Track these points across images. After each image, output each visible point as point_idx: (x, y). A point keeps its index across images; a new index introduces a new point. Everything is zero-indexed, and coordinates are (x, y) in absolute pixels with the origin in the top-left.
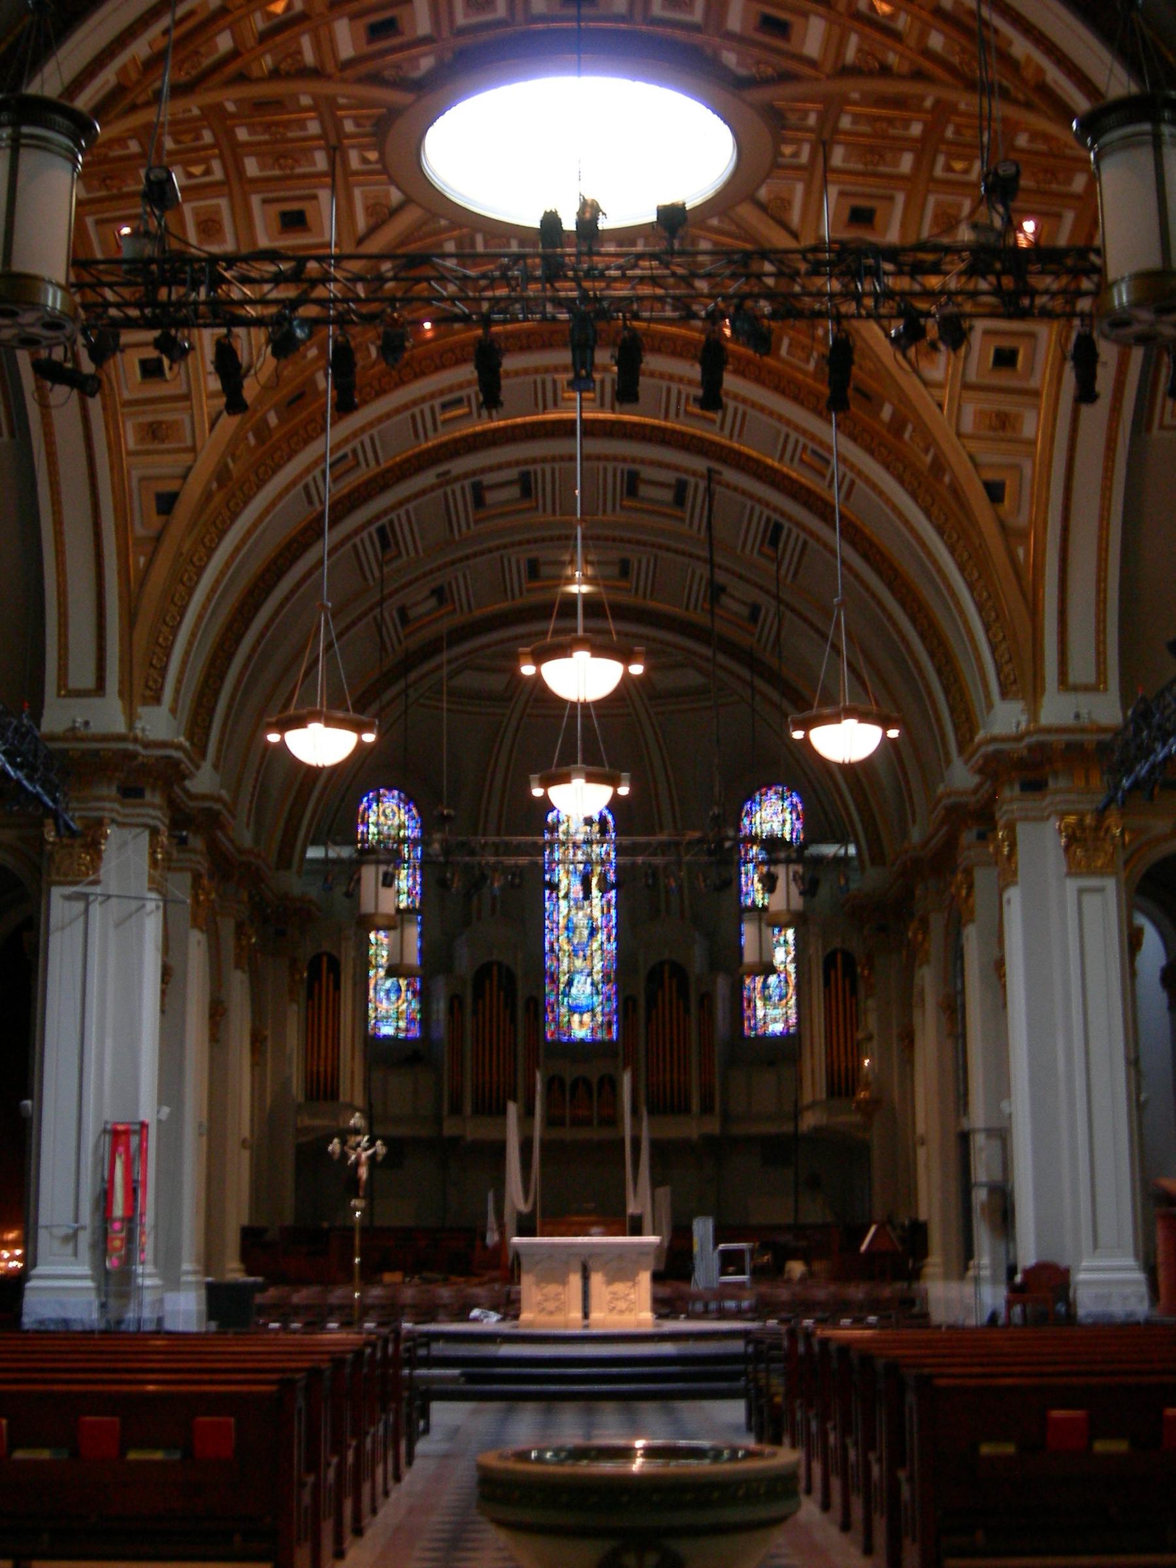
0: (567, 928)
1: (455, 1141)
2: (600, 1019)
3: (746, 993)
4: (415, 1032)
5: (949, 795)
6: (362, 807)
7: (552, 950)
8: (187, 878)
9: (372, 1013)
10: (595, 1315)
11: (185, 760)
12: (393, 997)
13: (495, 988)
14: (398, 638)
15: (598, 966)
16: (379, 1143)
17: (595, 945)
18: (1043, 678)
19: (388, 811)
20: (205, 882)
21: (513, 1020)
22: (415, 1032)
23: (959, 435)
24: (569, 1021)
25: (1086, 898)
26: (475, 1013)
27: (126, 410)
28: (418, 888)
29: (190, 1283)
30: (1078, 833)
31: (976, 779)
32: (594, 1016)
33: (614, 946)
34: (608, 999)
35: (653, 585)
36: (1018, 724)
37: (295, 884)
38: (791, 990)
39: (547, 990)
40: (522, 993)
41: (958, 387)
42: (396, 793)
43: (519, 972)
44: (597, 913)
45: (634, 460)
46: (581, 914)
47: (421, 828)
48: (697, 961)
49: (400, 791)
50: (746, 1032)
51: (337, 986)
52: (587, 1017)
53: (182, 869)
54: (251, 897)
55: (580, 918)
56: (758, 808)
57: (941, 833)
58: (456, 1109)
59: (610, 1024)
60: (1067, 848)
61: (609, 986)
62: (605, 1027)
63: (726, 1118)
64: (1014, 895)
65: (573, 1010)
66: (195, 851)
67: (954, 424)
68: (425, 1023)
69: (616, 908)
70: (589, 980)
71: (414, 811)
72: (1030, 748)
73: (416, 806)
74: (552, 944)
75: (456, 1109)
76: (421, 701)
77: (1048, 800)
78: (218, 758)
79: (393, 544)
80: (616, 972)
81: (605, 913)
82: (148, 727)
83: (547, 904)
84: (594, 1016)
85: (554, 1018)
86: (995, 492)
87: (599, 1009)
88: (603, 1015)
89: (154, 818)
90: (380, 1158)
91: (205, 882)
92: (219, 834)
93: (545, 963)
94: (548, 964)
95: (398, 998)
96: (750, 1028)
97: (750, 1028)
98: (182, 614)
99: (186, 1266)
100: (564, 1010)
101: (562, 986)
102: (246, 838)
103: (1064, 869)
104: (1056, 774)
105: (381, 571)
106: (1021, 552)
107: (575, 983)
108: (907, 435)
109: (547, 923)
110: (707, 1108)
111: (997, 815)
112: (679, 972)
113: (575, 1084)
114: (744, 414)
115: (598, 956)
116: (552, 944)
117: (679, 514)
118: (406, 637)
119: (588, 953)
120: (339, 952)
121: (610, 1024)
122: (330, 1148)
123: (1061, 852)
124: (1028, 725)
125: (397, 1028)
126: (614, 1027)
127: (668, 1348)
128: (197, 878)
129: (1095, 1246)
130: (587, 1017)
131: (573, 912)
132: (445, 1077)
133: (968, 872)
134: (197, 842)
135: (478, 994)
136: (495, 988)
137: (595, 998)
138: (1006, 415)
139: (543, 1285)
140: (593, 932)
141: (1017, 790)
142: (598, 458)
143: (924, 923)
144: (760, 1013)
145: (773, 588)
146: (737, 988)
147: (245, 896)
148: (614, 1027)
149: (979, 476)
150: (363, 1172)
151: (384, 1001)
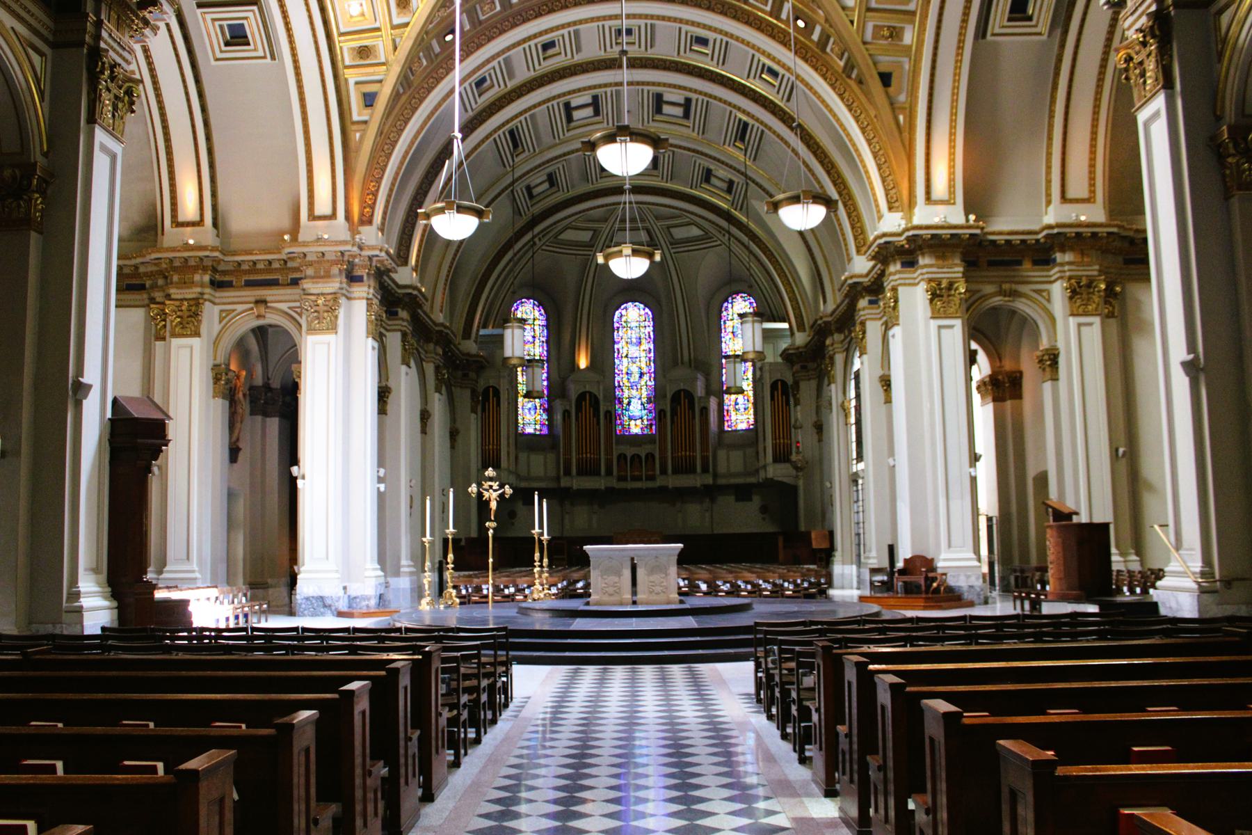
0: (627, 374)
1: (568, 490)
2: (646, 422)
3: (726, 408)
4: (545, 431)
5: (851, 277)
6: (513, 309)
7: (619, 386)
8: (399, 335)
9: (520, 421)
10: (640, 597)
12: (533, 412)
14: (528, 208)
15: (644, 394)
16: (507, 486)
17: (643, 383)
20: (409, 337)
21: (598, 423)
22: (545, 431)
23: (865, 43)
24: (629, 425)
26: (577, 419)
27: (342, 38)
28: (545, 353)
29: (406, 572)
31: (872, 263)
32: (643, 421)
34: (650, 412)
37: (470, 346)
38: (750, 405)
39: (617, 407)
41: (864, 10)
43: (601, 397)
44: (643, 365)
45: (659, 84)
46: (635, 365)
47: (546, 320)
48: (700, 390)
50: (726, 428)
51: (498, 404)
52: (639, 422)
54: (444, 352)
55: (634, 369)
56: (730, 306)
57: (846, 302)
58: (568, 472)
59: (651, 425)
60: (931, 301)
63: (715, 476)
65: (631, 418)
66: (403, 320)
67: (861, 35)
68: (550, 427)
69: (654, 363)
70: (640, 402)
71: (542, 311)
72: (909, 239)
73: (543, 308)
74: (619, 382)
75: (568, 472)
76: (544, 247)
77: (919, 271)
78: (383, 224)
80: (655, 397)
82: (364, 238)
83: (616, 360)
84: (643, 421)
86: (886, 79)
87: (645, 417)
88: (648, 420)
89: (402, 326)
91: (409, 337)
94: (617, 393)
96: (728, 426)
97: (728, 426)
99: (404, 562)
100: (626, 418)
102: (440, 317)
103: (929, 314)
104: (923, 254)
106: (901, 118)
108: (828, 50)
109: (616, 371)
110: (705, 470)
111: (885, 284)
112: (690, 396)
113: (633, 457)
114: (727, 43)
115: (644, 388)
116: (619, 382)
120: (499, 386)
121: (651, 425)
122: (470, 490)
125: (535, 429)
126: (654, 427)
128: (404, 335)
129: (949, 546)
130: (639, 422)
133: (863, 324)
134: (403, 314)
135: (579, 408)
138: (894, 28)
140: (641, 375)
141: (898, 266)
142: (638, 83)
143: (832, 358)
144: (733, 418)
145: (743, 170)
146: (721, 404)
148: (654, 427)
149: (877, 69)
150: (493, 505)
151: (528, 415)
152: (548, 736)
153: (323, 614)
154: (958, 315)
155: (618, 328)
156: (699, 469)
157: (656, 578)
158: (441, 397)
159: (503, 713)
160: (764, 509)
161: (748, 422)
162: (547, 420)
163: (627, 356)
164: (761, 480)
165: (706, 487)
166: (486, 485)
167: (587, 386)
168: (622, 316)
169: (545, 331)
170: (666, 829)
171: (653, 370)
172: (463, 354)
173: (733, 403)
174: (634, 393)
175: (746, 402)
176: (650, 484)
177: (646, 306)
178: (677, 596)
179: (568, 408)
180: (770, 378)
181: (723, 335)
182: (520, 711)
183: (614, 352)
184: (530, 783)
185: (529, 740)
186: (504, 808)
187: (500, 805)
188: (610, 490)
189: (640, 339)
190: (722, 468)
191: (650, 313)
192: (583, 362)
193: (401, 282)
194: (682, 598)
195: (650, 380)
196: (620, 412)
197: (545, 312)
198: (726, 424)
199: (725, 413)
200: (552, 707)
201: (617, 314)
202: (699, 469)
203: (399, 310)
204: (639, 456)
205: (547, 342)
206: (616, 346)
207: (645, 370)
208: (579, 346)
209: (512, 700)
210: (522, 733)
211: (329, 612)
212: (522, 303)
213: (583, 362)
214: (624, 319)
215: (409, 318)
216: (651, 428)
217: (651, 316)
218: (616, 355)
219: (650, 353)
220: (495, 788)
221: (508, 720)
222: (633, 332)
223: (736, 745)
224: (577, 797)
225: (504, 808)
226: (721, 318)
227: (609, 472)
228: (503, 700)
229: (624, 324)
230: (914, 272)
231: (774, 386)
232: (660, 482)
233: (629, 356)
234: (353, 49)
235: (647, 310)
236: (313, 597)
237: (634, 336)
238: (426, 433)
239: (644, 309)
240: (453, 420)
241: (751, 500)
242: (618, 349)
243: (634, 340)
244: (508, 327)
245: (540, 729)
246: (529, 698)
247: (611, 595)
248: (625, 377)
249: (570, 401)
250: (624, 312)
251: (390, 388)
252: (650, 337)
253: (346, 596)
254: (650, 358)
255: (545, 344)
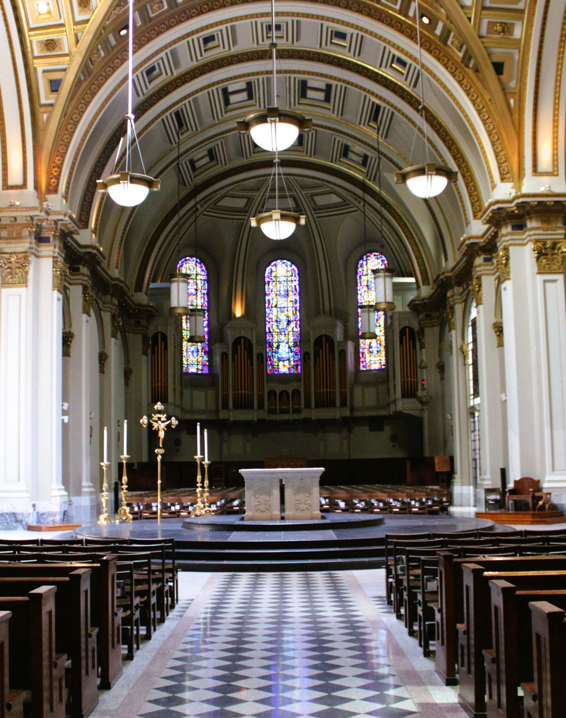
0: (277, 321)
2: (292, 363)
3: (361, 350)
4: (206, 371)
5: (469, 238)
6: (178, 265)
7: (270, 332)
8: (80, 288)
11: (98, 254)
12: (195, 354)
13: (243, 348)
15: (291, 339)
16: (173, 418)
17: (290, 329)
18: (524, 169)
19: (191, 267)
21: (252, 364)
22: (206, 371)
23: (480, 37)
24: (278, 365)
25: (548, 285)
28: (206, 303)
29: (86, 492)
30: (543, 251)
33: (299, 329)
34: (296, 354)
35: (315, 150)
36: (510, 194)
39: (268, 350)
40: (255, 352)
41: (480, 8)
42: (195, 259)
43: (254, 342)
44: (290, 314)
46: (283, 314)
47: (207, 275)
48: (339, 335)
49: (197, 258)
50: (362, 368)
51: (166, 348)
52: (286, 363)
53: (77, 284)
55: (283, 317)
56: (365, 263)
58: (225, 406)
59: (297, 365)
60: (538, 258)
61: (297, 348)
62: (295, 367)
63: (352, 409)
64: (507, 285)
65: (279, 360)
66: (84, 275)
67: (477, 30)
68: (210, 367)
69: (300, 312)
70: (287, 346)
71: (204, 268)
72: (518, 205)
73: (204, 265)
74: (269, 328)
75: (225, 406)
76: (205, 213)
79: (184, 125)
80: (300, 341)
81: (295, 314)
82: (50, 205)
83: (267, 310)
84: (290, 362)
85: (271, 364)
87: (292, 359)
88: (294, 361)
90: (173, 427)
92: (98, 267)
93: (266, 337)
94: (268, 338)
95: (197, 355)
96: (363, 367)
97: (363, 367)
98: (67, 147)
99: (85, 483)
100: (275, 360)
101: (274, 348)
102: (116, 273)
103: (536, 270)
105: (179, 138)
106: (512, 101)
107: (280, 347)
108: (449, 43)
110: (343, 404)
111: (498, 244)
112: (330, 340)
113: (281, 393)
115: (291, 333)
116: (269, 328)
117: (328, 107)
118: (195, 177)
119: (287, 333)
121: (297, 365)
122: (141, 421)
123: (535, 259)
124: (516, 193)
125: (198, 369)
126: (299, 367)
127: (330, 535)
128: (85, 288)
129: (553, 469)
130: (286, 363)
131: (279, 313)
132: (220, 390)
133: (479, 278)
134: (84, 270)
136: (243, 348)
137: (290, 354)
138: (506, 24)
139: (257, 496)
140: (289, 322)
141: (509, 229)
144: (368, 359)
147: (116, 302)
148: (299, 367)
149: (491, 59)
150: (162, 434)
152: (208, 633)
153: (15, 528)
154: (560, 271)
155: (269, 282)
156: (338, 403)
157: (301, 497)
158: (88, 318)
159: (169, 613)
160: (394, 438)
161: (380, 363)
162: (208, 361)
163: (276, 306)
164: (391, 413)
165: (344, 419)
166: (155, 417)
167: (242, 332)
168: (272, 271)
169: (206, 285)
170: (310, 713)
171: (298, 318)
172: (136, 305)
173: (367, 347)
174: (282, 338)
175: (379, 346)
176: (296, 417)
177: (293, 263)
178: (319, 512)
179: (226, 351)
180: (399, 325)
181: (358, 288)
182: (184, 612)
183: (265, 303)
184: (193, 673)
185: (192, 636)
186: (170, 695)
187: (167, 692)
188: (262, 422)
189: (287, 291)
190: (358, 403)
191: (296, 269)
192: (238, 312)
193: (82, 243)
194: (324, 514)
195: (296, 327)
196: (270, 354)
197: (206, 269)
198: (361, 365)
199: (361, 356)
200: (212, 608)
201: (268, 269)
202: (338, 403)
203: (81, 267)
204: (287, 393)
205: (208, 294)
206: (267, 298)
207: (292, 318)
208: (235, 298)
209: (177, 602)
210: (186, 630)
211: (21, 526)
212: (186, 260)
213: (238, 312)
214: (273, 274)
215: (89, 274)
216: (297, 368)
217: (297, 272)
218: (267, 305)
219: (296, 303)
220: (163, 678)
221: (174, 619)
222: (282, 286)
223: (369, 641)
224: (234, 685)
225: (170, 695)
226: (357, 274)
227: (261, 406)
228: (170, 602)
229: (274, 279)
230: (523, 234)
231: (402, 332)
232: (304, 414)
233: (278, 306)
234: (41, 42)
235: (294, 267)
236: (6, 513)
237: (282, 289)
238: (103, 373)
239: (291, 266)
240: (127, 360)
241: (383, 430)
242: (269, 300)
243: (283, 293)
244: (174, 282)
245: (202, 627)
246: (192, 600)
247: (262, 512)
248: (275, 324)
249: (227, 345)
250: (274, 269)
251: (73, 334)
252: (296, 290)
253: (35, 513)
254: (296, 308)
255: (206, 296)
